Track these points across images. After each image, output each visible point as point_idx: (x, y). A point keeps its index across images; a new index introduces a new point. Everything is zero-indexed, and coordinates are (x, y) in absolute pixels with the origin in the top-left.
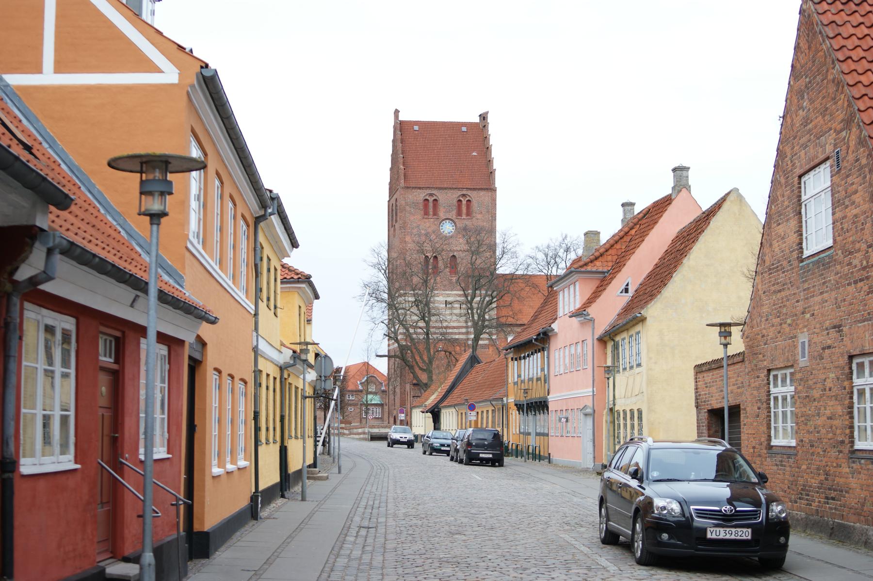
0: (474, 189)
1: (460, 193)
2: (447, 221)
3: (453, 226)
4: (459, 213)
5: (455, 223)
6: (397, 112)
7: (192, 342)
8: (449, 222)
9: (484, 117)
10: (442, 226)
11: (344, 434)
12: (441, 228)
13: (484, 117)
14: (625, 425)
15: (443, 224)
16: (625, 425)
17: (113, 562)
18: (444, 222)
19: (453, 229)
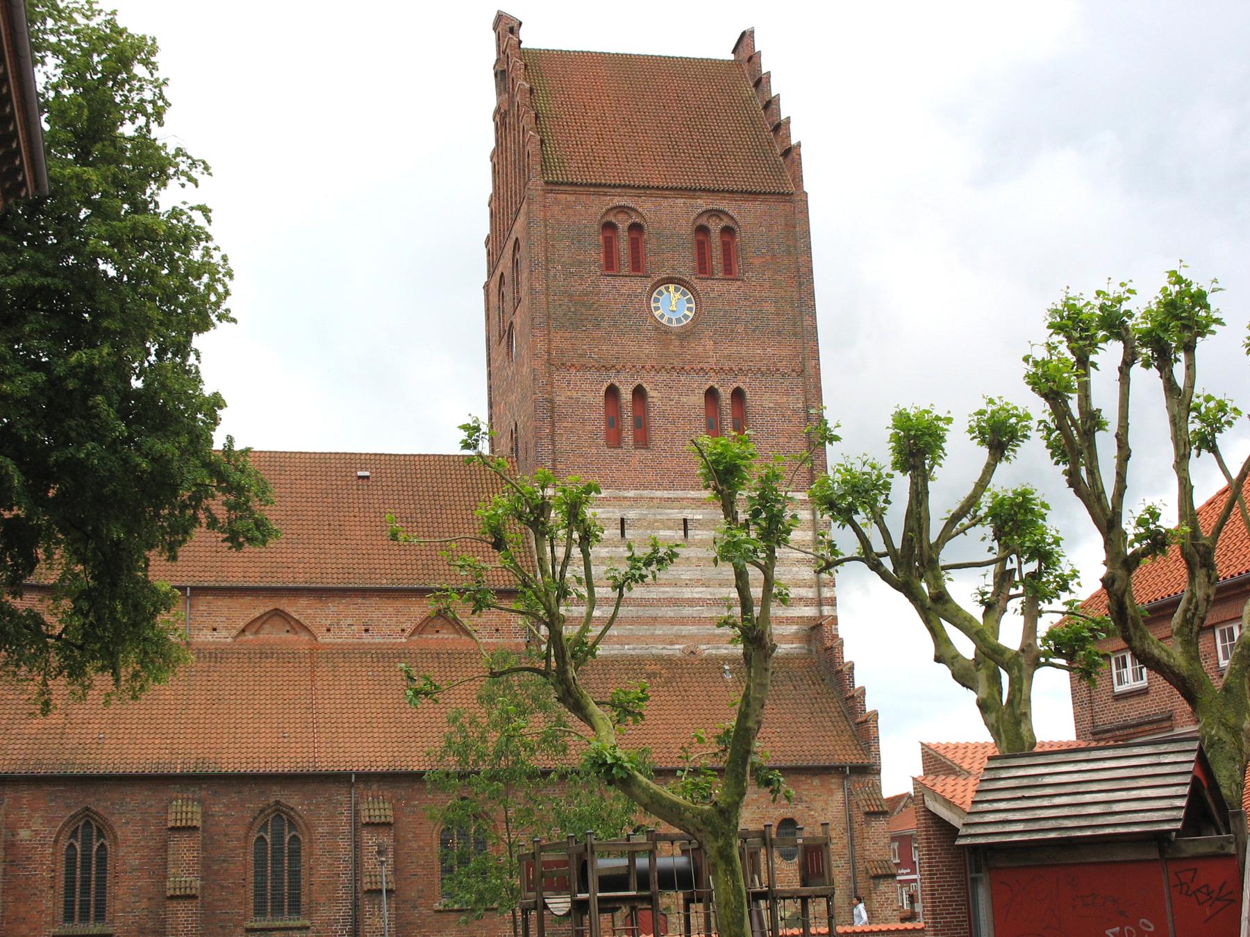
0: (753, 194)
1: (702, 203)
2: (672, 287)
3: (689, 301)
4: (703, 268)
5: (692, 289)
6: (506, 28)
7: (198, 341)
8: (676, 290)
9: (745, 39)
10: (657, 300)
11: (294, 839)
12: (653, 305)
13: (745, 39)
14: (673, 622)
15: (661, 293)
16: (673, 622)
17: (261, 626)
18: (662, 288)
19: (689, 309)
